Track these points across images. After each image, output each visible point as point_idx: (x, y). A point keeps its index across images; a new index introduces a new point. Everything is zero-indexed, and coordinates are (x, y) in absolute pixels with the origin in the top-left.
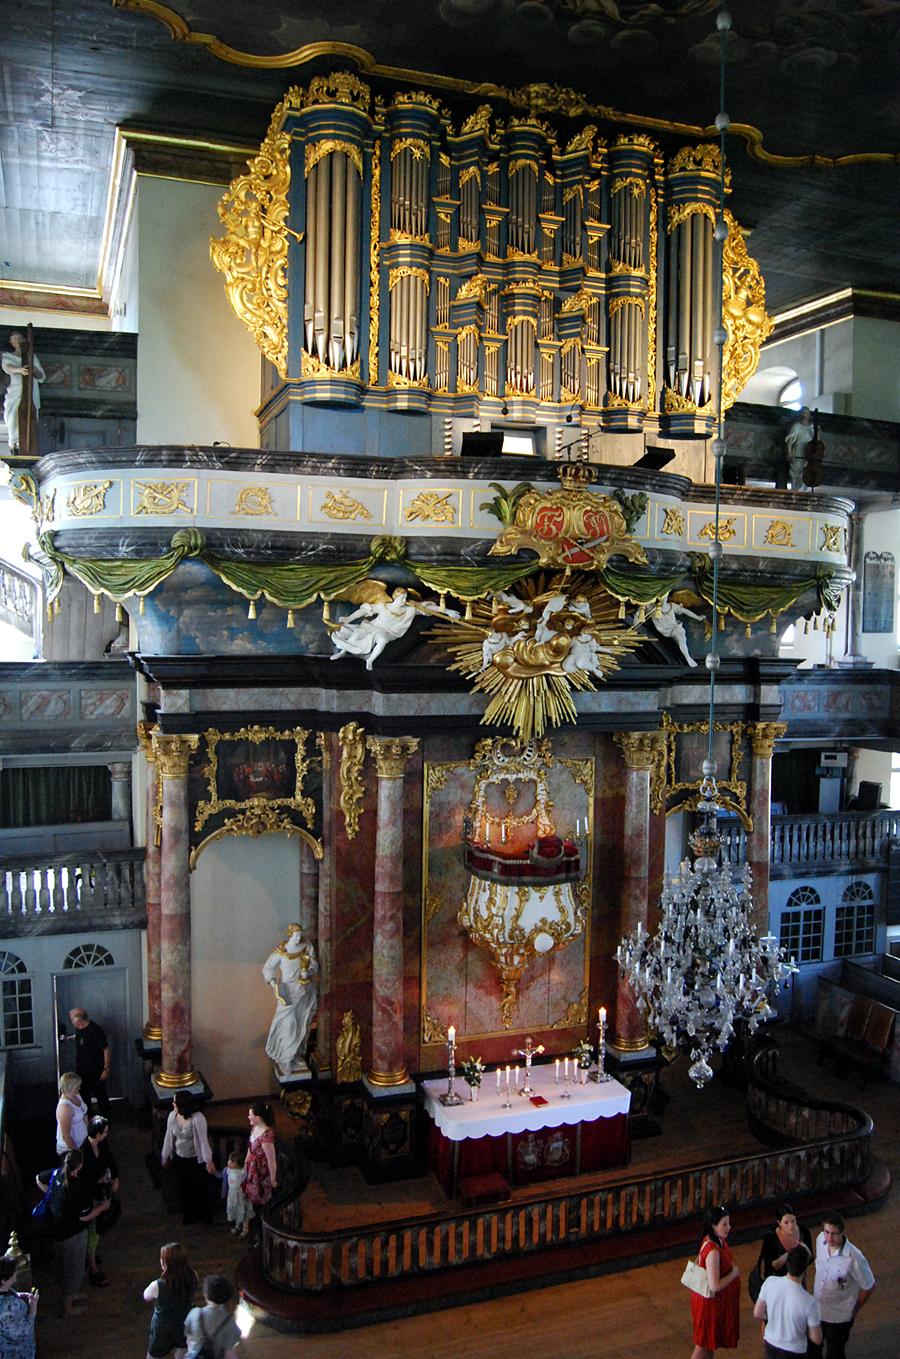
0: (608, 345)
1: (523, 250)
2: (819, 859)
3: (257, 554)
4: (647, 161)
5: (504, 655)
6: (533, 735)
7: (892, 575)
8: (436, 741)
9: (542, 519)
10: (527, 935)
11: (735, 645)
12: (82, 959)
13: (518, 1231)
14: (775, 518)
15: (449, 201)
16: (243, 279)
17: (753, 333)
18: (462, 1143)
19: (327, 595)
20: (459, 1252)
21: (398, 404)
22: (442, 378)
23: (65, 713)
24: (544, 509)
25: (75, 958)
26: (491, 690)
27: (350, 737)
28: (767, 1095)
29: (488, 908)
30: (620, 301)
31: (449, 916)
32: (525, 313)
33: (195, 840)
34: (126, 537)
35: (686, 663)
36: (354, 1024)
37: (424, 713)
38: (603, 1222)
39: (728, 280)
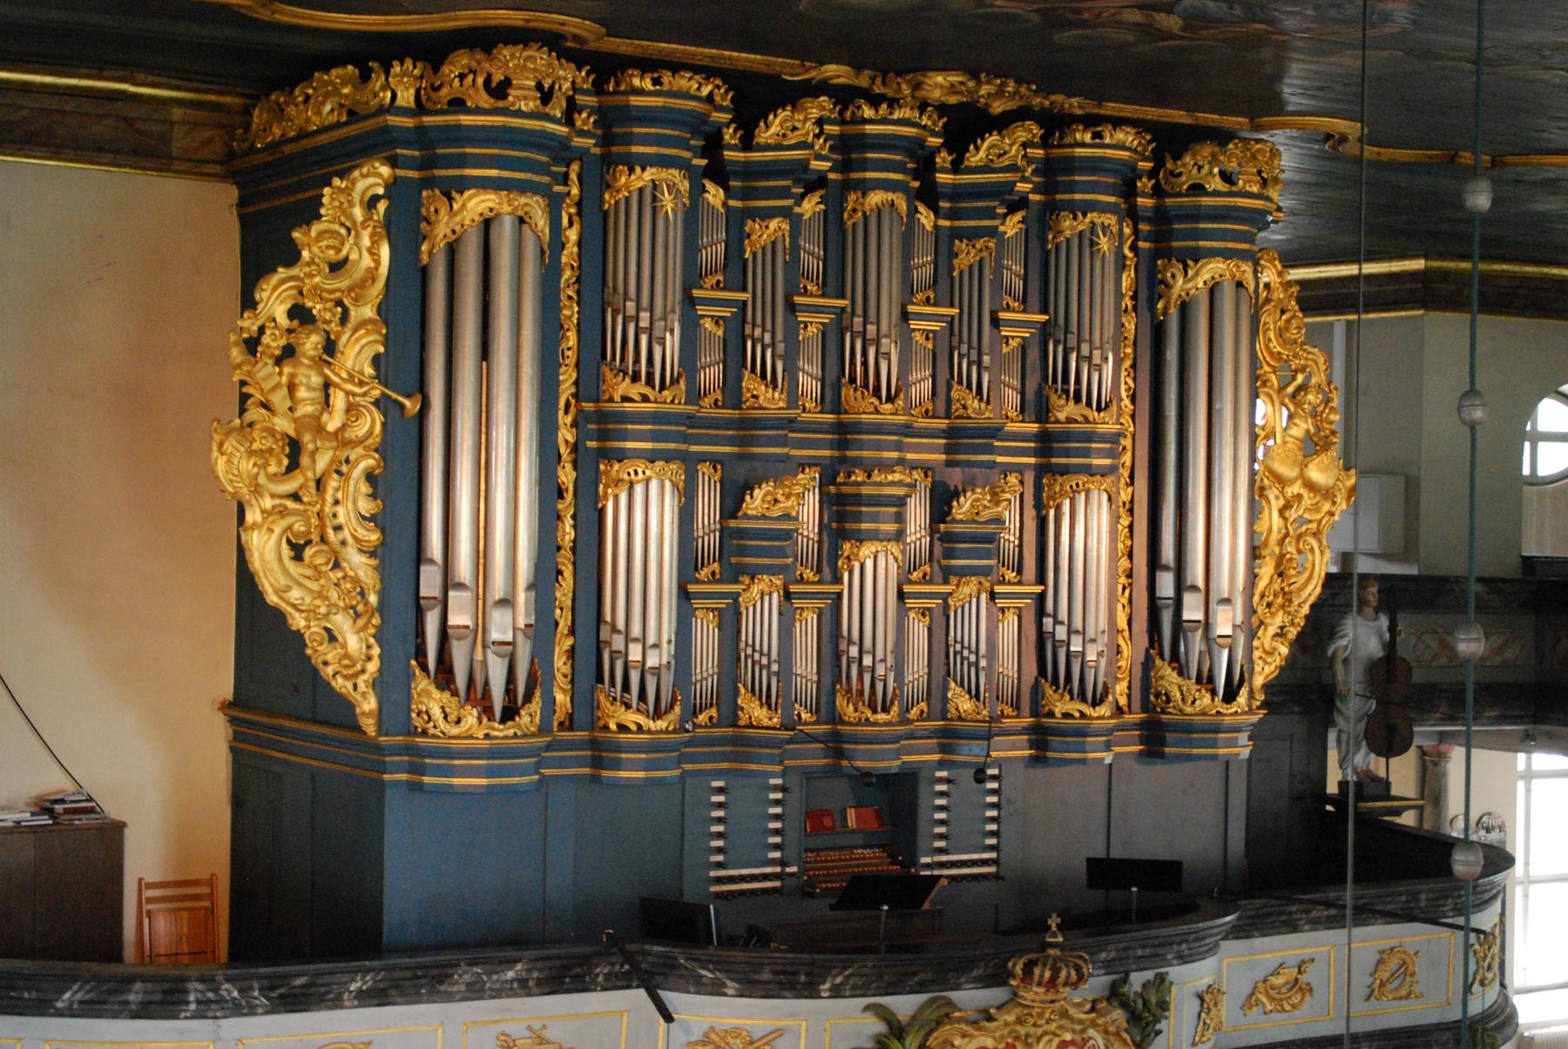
14: (1386, 944)
17: (1316, 508)
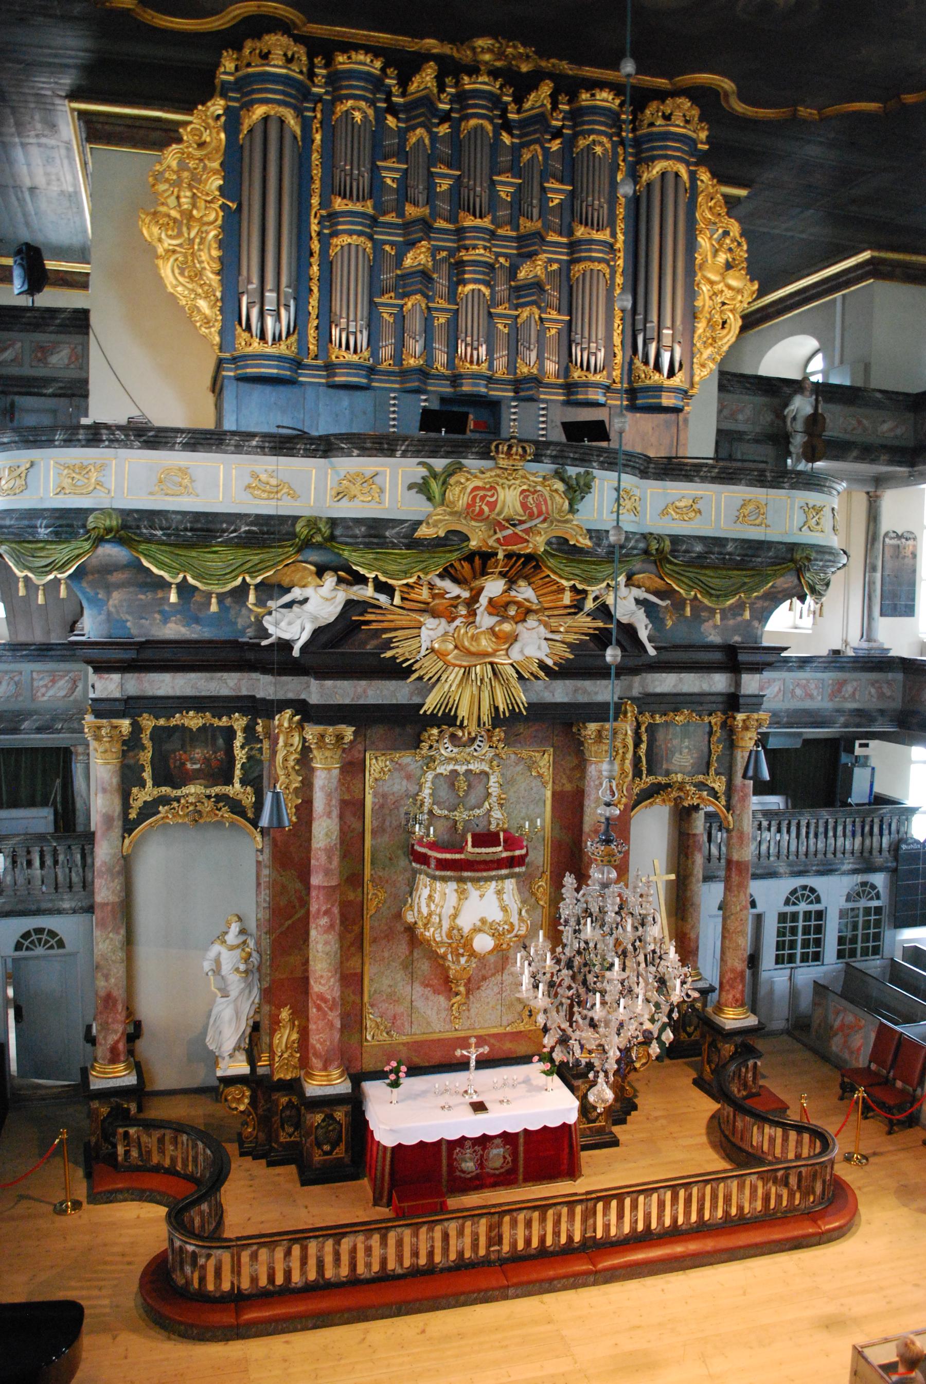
0: (570, 314)
1: (474, 215)
2: (820, 856)
3: (178, 536)
4: (613, 118)
5: (444, 641)
6: (479, 726)
7: (914, 556)
8: (377, 732)
9: (474, 498)
10: (465, 935)
11: (713, 632)
12: (32, 942)
13: (432, 1247)
14: (748, 497)
15: (396, 165)
16: (174, 252)
17: (733, 299)
18: (393, 1148)
19: (252, 577)
20: (368, 1265)
21: (337, 379)
22: (441, 358)
23: (17, 695)
24: (476, 488)
25: (25, 941)
26: (430, 678)
27: (286, 724)
28: (735, 1110)
29: (428, 906)
30: (581, 266)
31: (394, 911)
32: (476, 281)
33: (129, 827)
34: (45, 518)
35: (646, 652)
36: (292, 1021)
37: (361, 702)
38: (528, 1242)
39: (704, 242)
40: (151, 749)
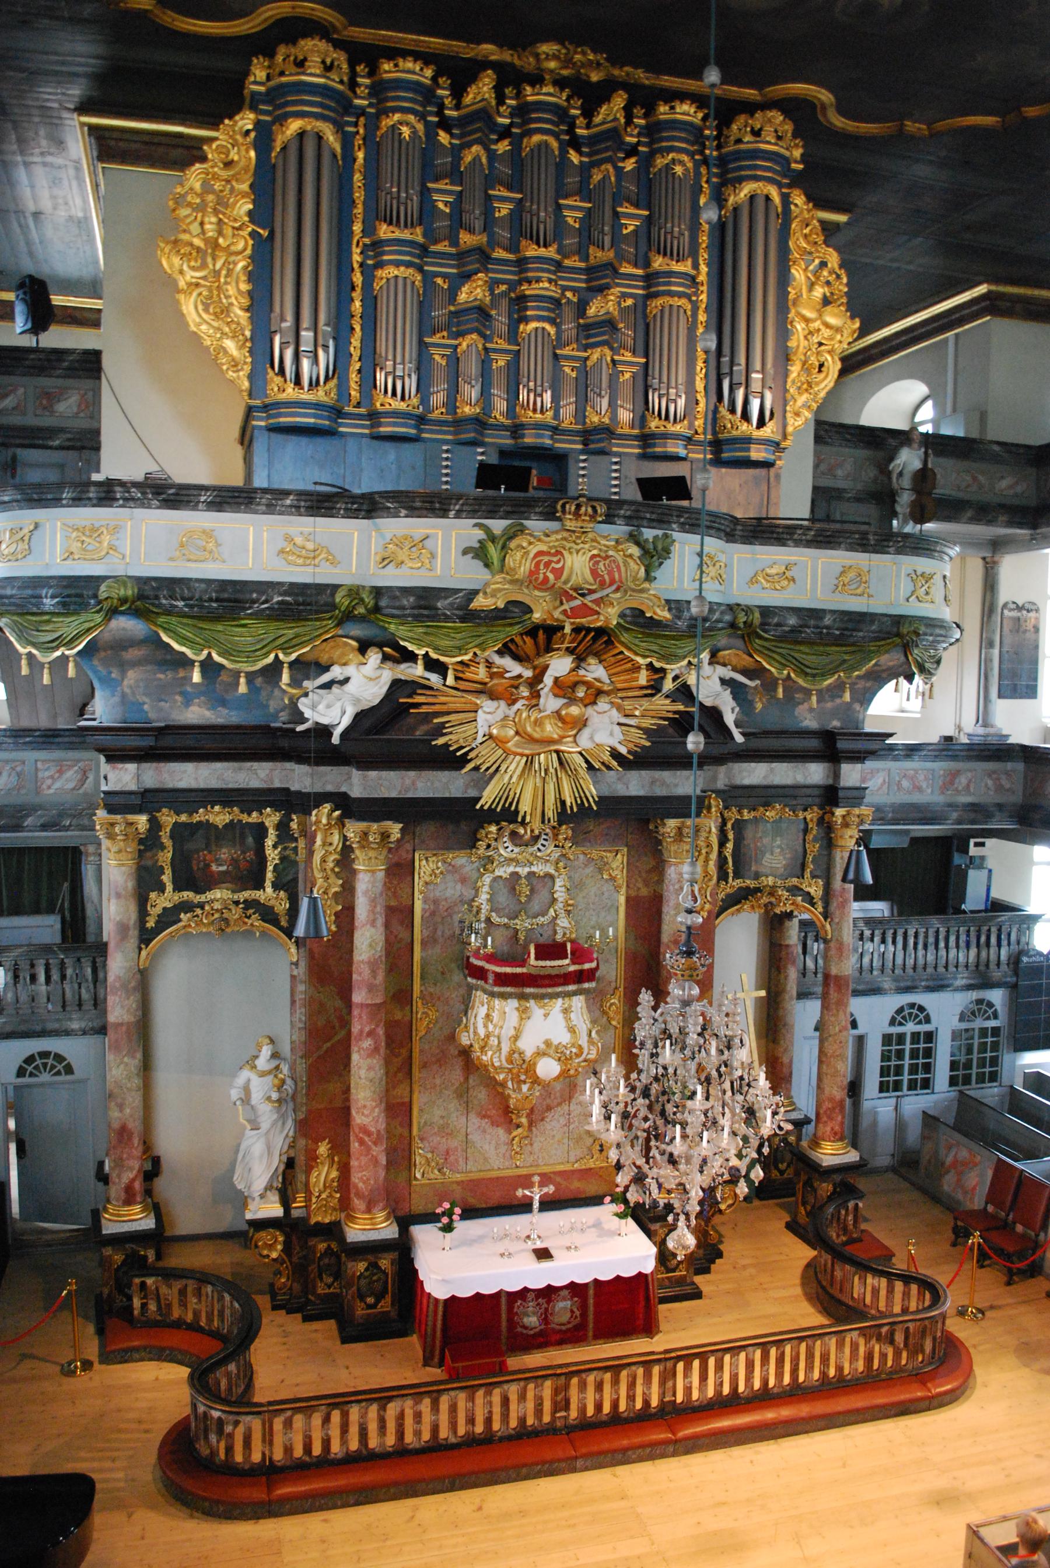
0: (647, 356)
1: (538, 244)
2: (930, 970)
3: (201, 607)
4: (696, 134)
5: (504, 726)
6: (543, 822)
7: (1037, 630)
8: (427, 829)
9: (537, 564)
10: (527, 1059)
11: (808, 716)
12: (36, 1068)
13: (490, 1412)
14: (848, 563)
15: (449, 187)
16: (197, 285)
17: (831, 339)
18: (446, 1301)
19: (286, 654)
20: (418, 1433)
21: (382, 429)
22: (500, 405)
23: (19, 788)
24: (540, 553)
25: (28, 1066)
26: (488, 769)
27: (324, 821)
28: (833, 1258)
29: (485, 1026)
30: (659, 302)
31: (447, 1032)
32: (539, 319)
33: (146, 937)
34: (51, 587)
35: (732, 738)
36: (331, 1157)
37: (410, 795)
38: (599, 1407)
39: (798, 274)
40: (171, 849)
